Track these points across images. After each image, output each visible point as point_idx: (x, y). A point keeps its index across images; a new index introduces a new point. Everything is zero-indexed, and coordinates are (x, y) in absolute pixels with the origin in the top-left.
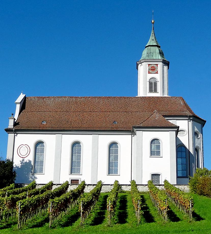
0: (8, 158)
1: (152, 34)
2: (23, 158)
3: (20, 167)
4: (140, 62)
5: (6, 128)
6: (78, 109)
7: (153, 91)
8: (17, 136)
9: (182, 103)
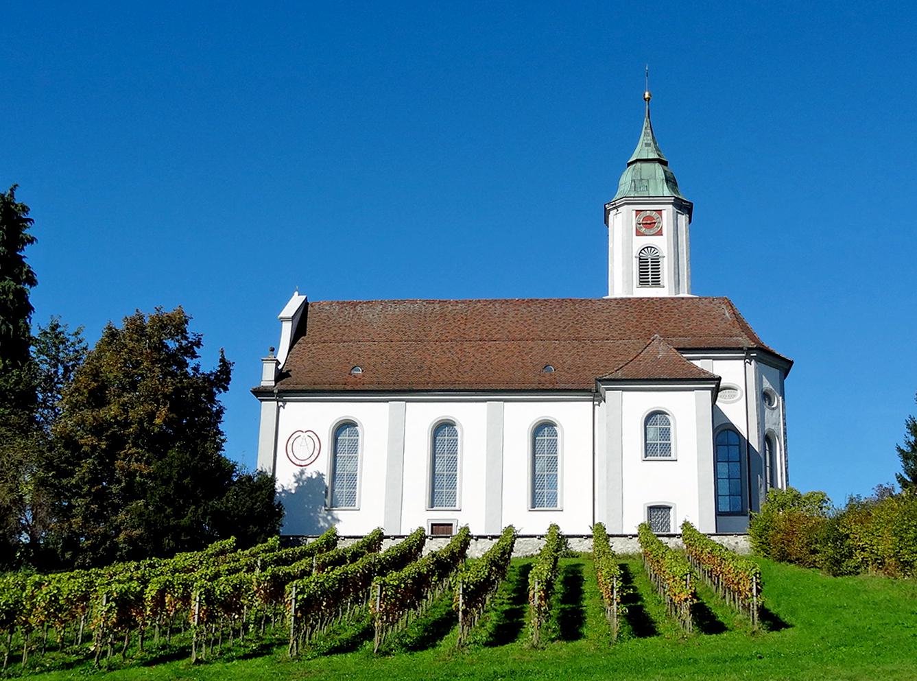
0: (262, 468)
1: (644, 128)
2: (301, 468)
3: (293, 492)
4: (613, 205)
5: (255, 387)
6: (447, 334)
7: (650, 284)
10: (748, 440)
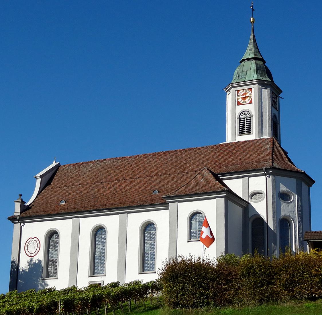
0: (13, 260)
2: (31, 258)
3: (27, 271)
5: (9, 216)
8: (24, 227)
9: (269, 148)
10: (267, 224)
